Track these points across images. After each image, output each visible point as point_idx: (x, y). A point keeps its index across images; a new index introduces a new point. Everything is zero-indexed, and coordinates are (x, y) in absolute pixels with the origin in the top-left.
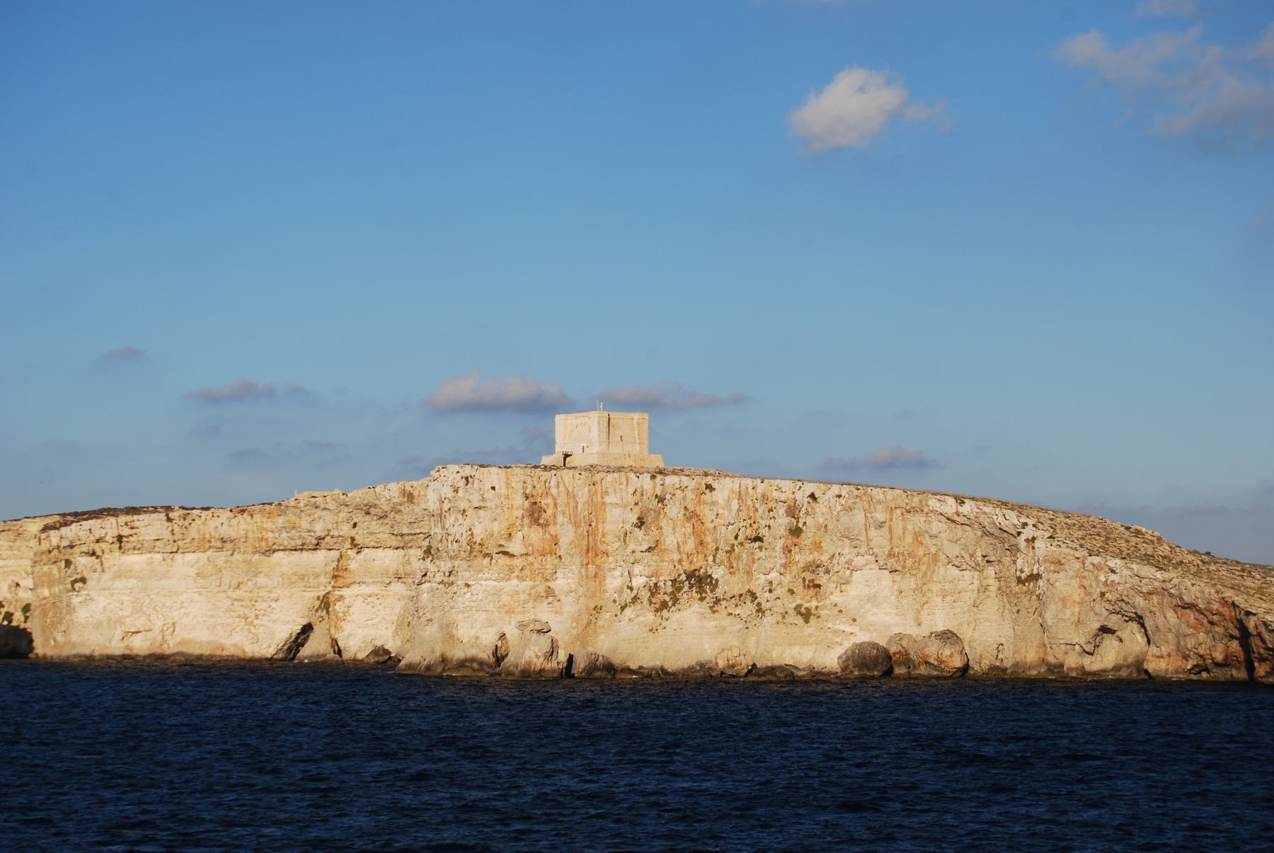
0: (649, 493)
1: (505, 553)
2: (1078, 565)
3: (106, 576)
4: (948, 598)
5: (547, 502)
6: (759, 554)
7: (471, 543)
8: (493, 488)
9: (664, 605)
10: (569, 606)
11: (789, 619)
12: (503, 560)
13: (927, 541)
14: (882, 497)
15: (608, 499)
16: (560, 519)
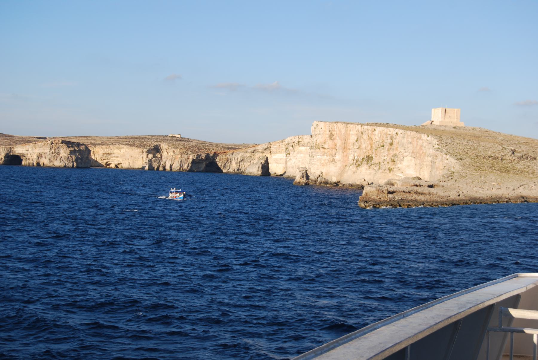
0: (360, 131)
1: (323, 148)
2: (441, 157)
5: (334, 133)
6: (382, 151)
7: (316, 144)
9: (359, 165)
10: (339, 164)
11: (386, 171)
12: (322, 150)
13: (423, 148)
15: (351, 133)
16: (337, 138)
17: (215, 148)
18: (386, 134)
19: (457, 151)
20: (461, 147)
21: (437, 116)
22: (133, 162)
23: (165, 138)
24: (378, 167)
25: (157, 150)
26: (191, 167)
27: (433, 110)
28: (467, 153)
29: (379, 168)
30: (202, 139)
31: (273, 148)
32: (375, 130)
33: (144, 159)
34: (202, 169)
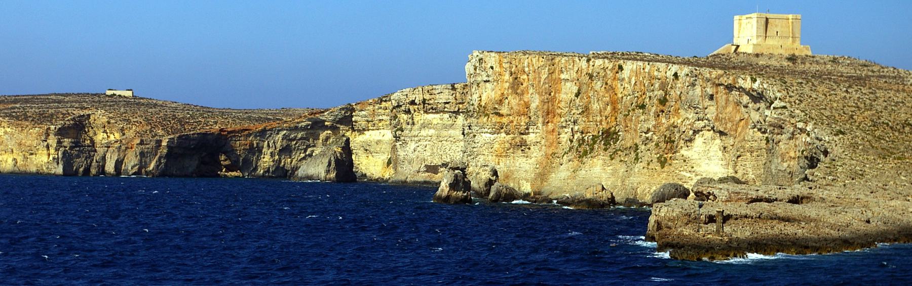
3: (416, 127)
4: (755, 154)
6: (642, 117)
8: (492, 68)
9: (585, 153)
10: (536, 154)
11: (651, 166)
12: (495, 119)
14: (708, 76)
17: (220, 119)
18: (652, 78)
19: (827, 113)
20: (835, 105)
21: (746, 35)
22: (25, 158)
23: (100, 100)
24: (633, 155)
25: (77, 129)
26: (166, 164)
27: (736, 18)
28: (852, 117)
29: (637, 159)
30: (182, 100)
31: (359, 118)
32: (621, 68)
33: (52, 151)
34: (191, 170)
